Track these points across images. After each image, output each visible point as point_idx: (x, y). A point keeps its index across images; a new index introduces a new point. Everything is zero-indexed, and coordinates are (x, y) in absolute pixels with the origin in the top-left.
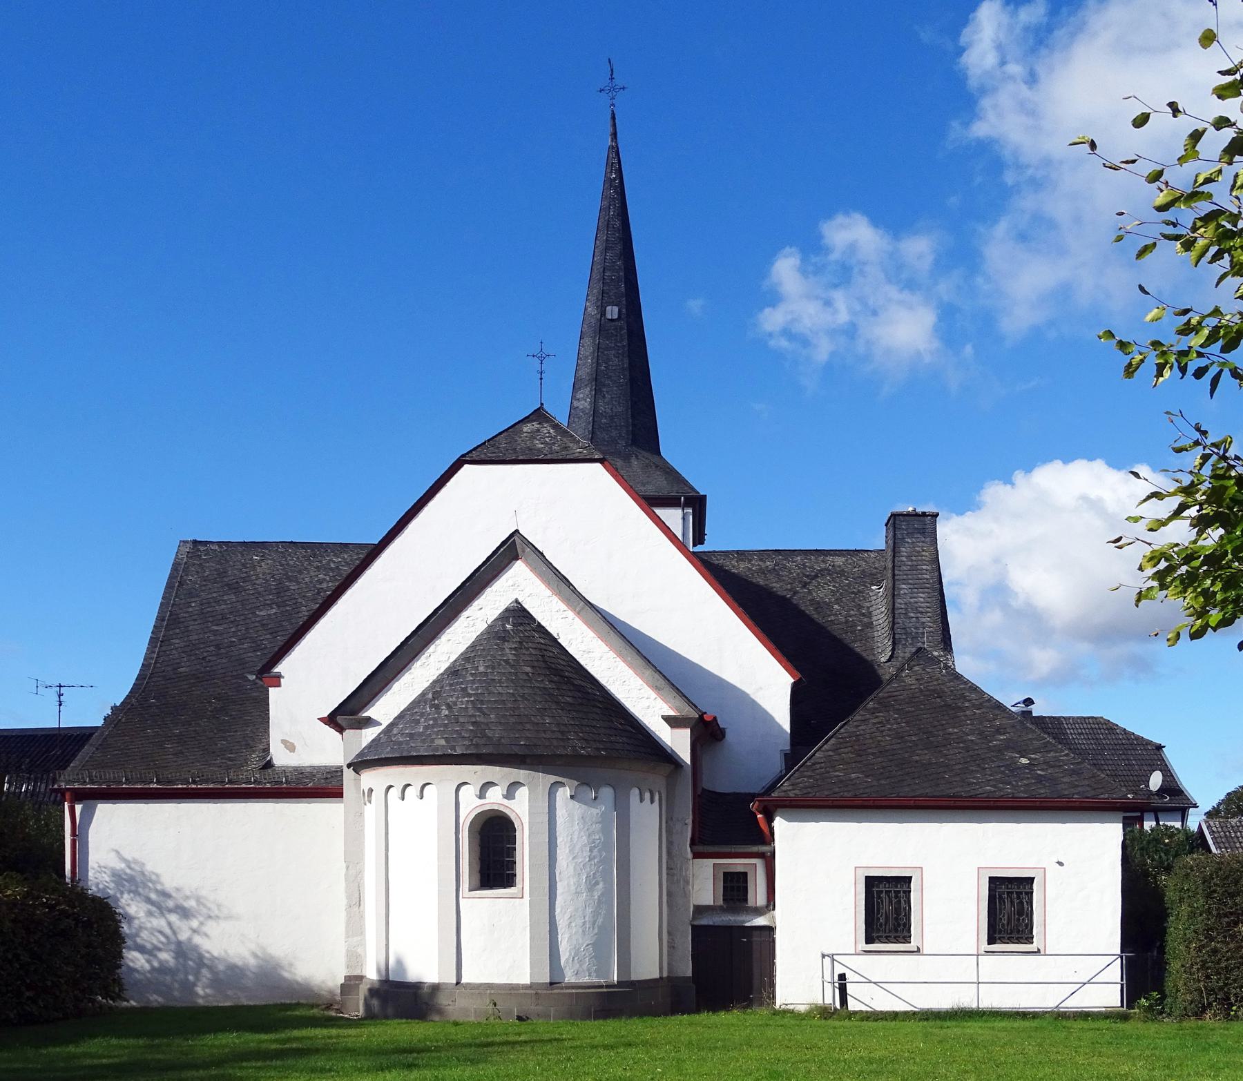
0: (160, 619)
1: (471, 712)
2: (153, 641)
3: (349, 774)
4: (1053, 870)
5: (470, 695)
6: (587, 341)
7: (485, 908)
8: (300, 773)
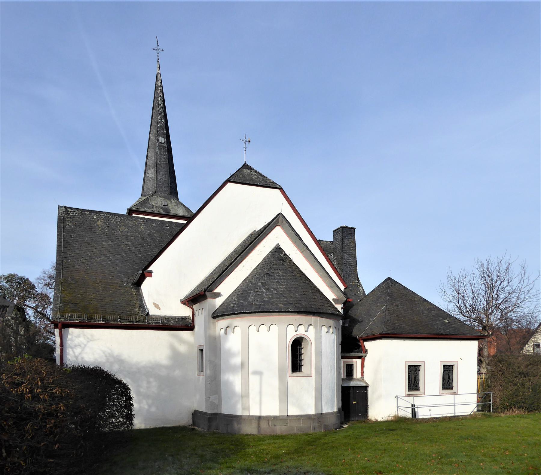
4: (460, 361)
7: (295, 381)
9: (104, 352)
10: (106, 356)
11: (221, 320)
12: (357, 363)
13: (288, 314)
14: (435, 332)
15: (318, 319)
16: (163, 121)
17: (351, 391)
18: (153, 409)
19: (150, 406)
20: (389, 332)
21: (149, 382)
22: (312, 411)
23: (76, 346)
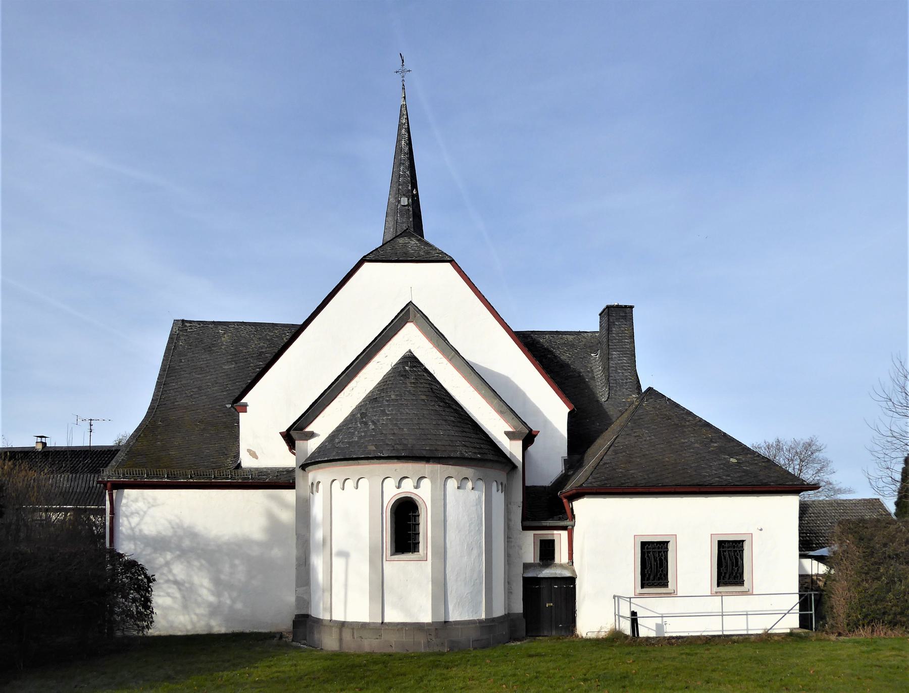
0: (163, 369)
1: (391, 427)
2: (159, 384)
3: (299, 473)
5: (388, 415)
6: (390, 219)
8: (261, 472)
9: (170, 523)
10: (173, 528)
12: (561, 537)
13: (375, 461)
14: (696, 482)
15: (438, 467)
16: (408, 173)
17: (544, 585)
18: (239, 606)
19: (234, 601)
20: (595, 484)
21: (233, 566)
22: (426, 618)
23: (132, 513)
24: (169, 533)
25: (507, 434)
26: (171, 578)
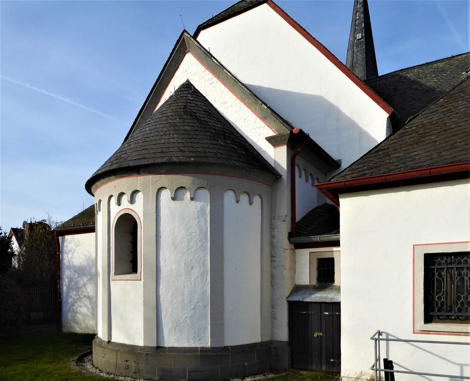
6: (350, 52)
9: (85, 256)
10: (87, 260)
11: (107, 182)
15: (150, 178)
16: (362, 16)
22: (139, 341)
23: (69, 251)
24: (85, 264)
25: (269, 139)
26: (87, 295)
